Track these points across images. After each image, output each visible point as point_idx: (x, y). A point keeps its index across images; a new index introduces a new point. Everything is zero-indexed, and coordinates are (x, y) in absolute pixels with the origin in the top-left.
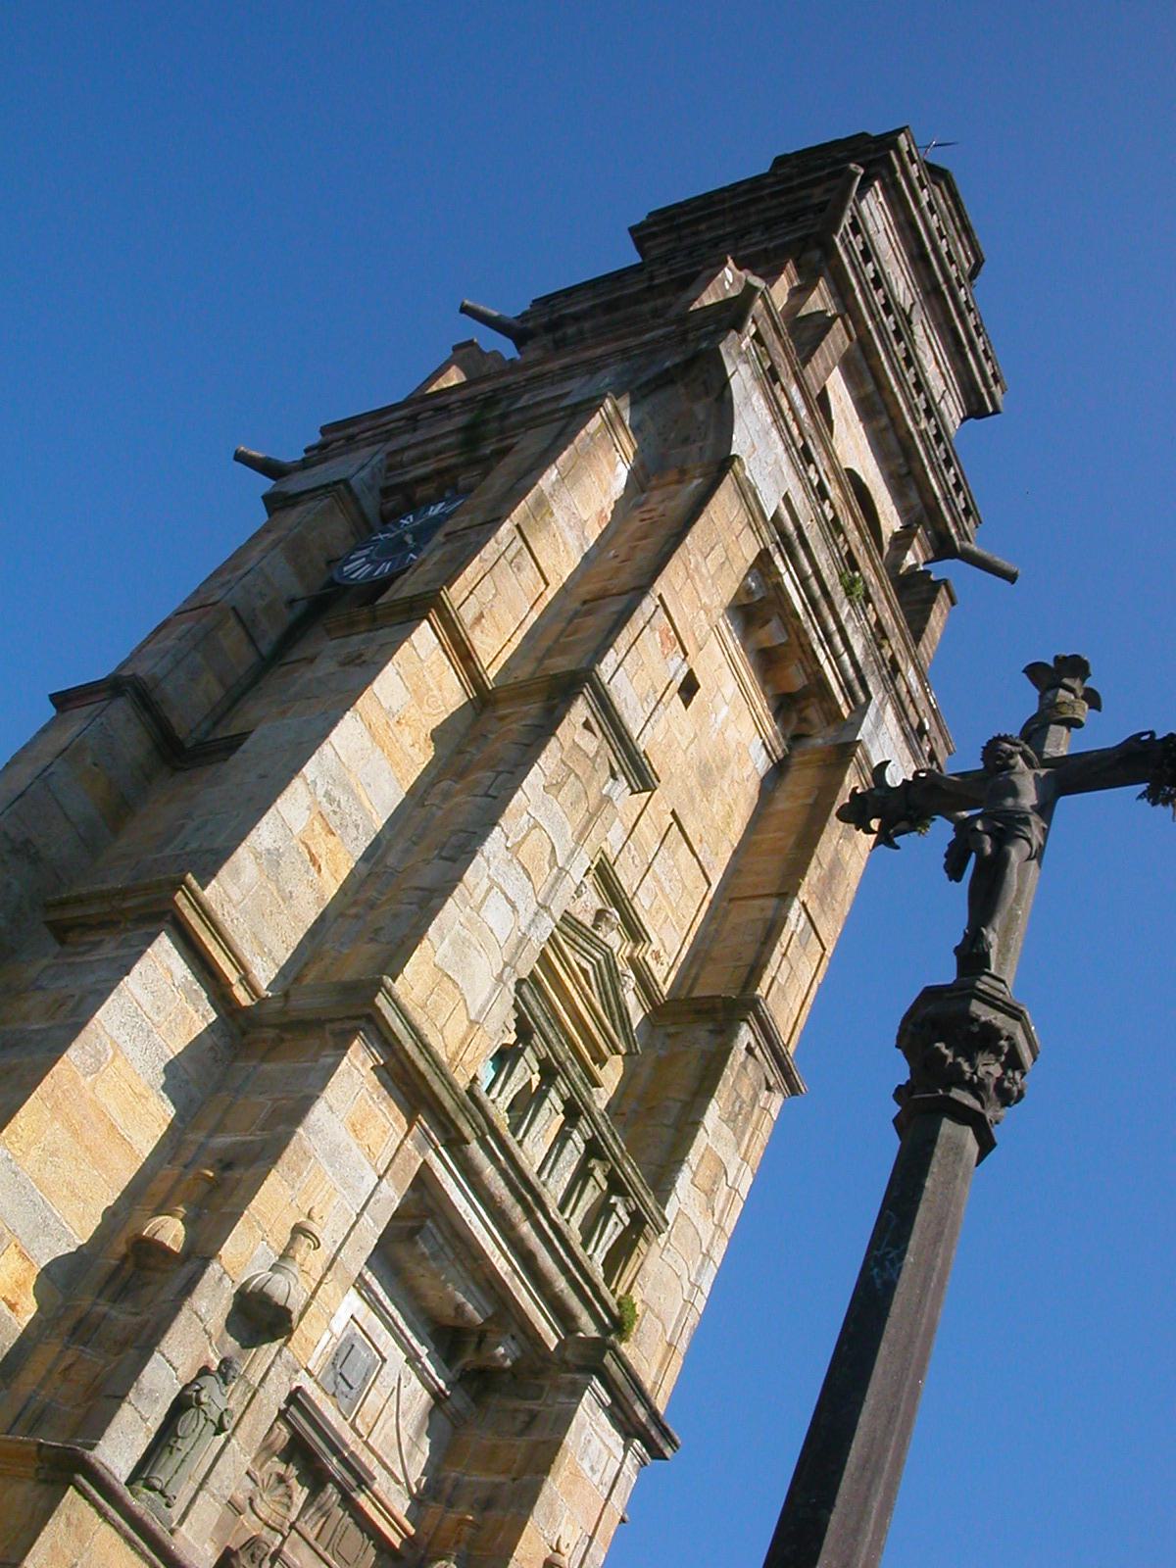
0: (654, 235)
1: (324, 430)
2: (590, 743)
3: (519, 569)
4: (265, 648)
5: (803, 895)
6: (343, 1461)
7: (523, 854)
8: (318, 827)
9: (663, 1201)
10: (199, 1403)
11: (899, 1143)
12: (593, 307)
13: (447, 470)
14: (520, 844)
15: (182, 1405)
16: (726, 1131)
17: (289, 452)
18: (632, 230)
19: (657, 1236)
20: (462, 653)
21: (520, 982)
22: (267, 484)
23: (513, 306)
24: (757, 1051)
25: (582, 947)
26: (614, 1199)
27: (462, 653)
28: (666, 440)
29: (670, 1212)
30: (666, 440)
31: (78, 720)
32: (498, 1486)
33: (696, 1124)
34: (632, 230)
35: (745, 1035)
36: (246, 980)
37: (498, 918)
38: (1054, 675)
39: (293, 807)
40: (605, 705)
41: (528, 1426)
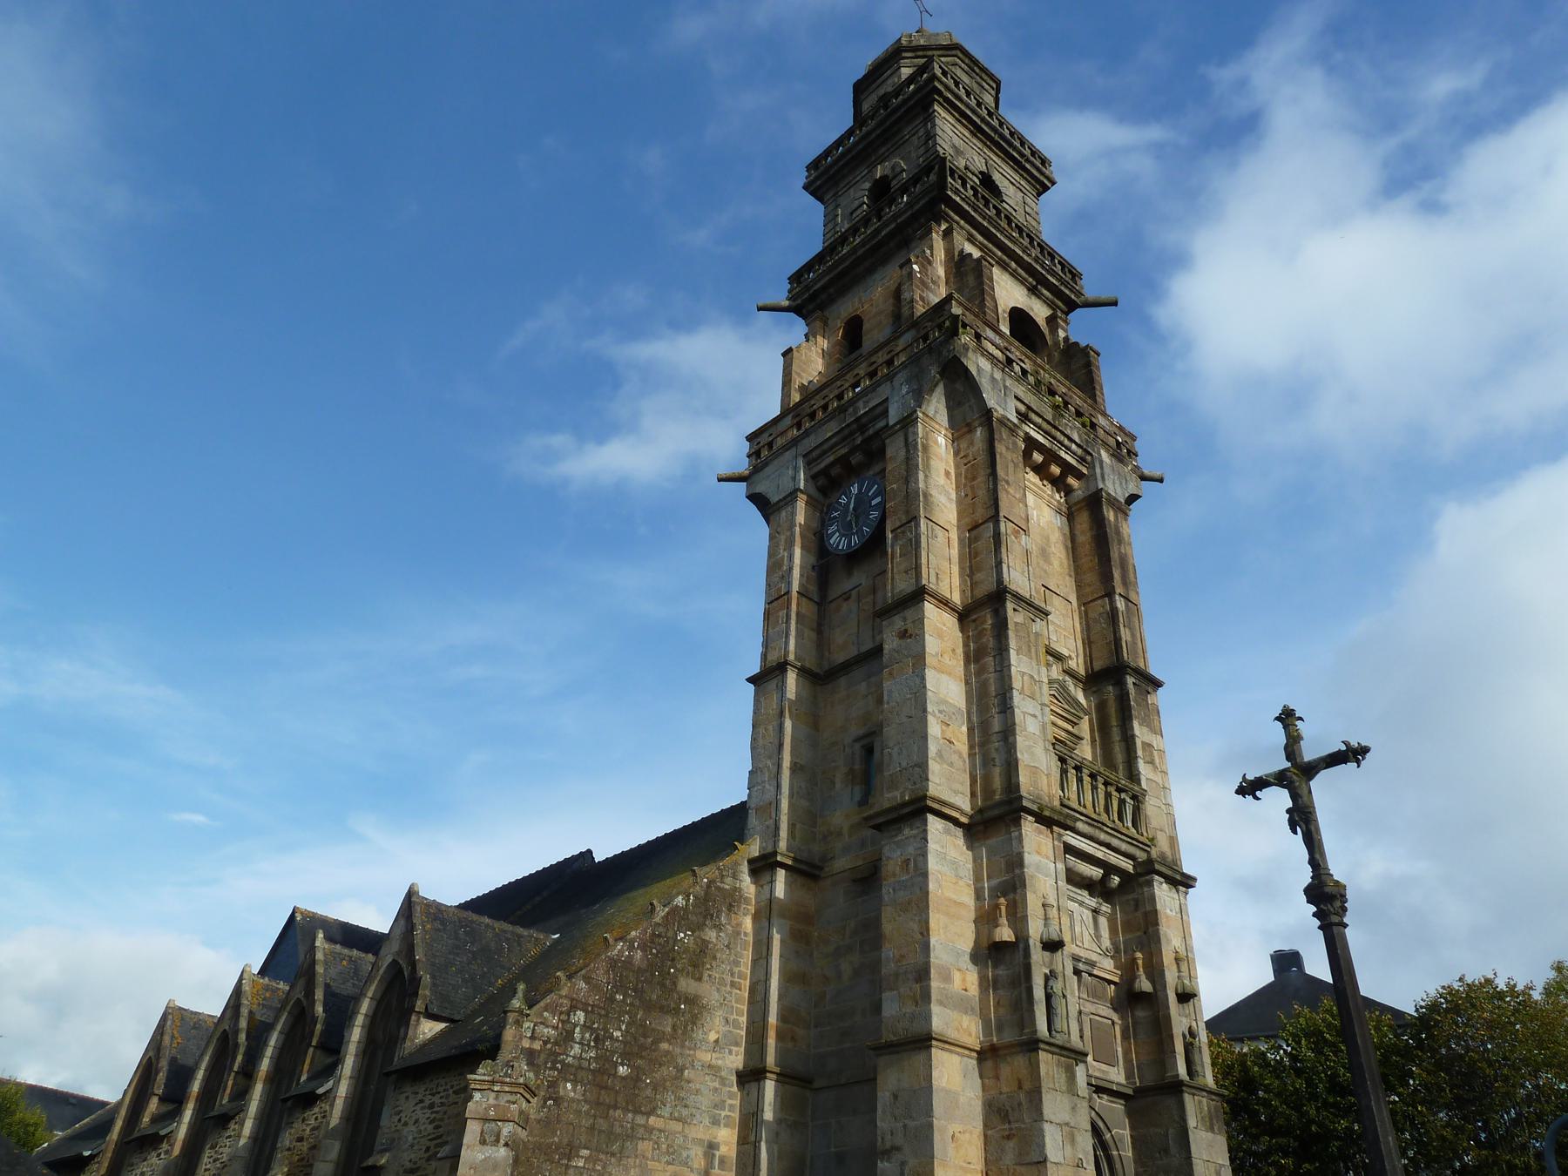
0: (819, 187)
5: (1118, 590)
11: (1363, 992)
18: (806, 188)
20: (944, 603)
25: (825, 452)
27: (944, 603)
29: (1144, 786)
33: (1133, 736)
34: (806, 188)
35: (1130, 680)
36: (962, 812)
38: (1287, 717)
39: (934, 728)
40: (1018, 598)
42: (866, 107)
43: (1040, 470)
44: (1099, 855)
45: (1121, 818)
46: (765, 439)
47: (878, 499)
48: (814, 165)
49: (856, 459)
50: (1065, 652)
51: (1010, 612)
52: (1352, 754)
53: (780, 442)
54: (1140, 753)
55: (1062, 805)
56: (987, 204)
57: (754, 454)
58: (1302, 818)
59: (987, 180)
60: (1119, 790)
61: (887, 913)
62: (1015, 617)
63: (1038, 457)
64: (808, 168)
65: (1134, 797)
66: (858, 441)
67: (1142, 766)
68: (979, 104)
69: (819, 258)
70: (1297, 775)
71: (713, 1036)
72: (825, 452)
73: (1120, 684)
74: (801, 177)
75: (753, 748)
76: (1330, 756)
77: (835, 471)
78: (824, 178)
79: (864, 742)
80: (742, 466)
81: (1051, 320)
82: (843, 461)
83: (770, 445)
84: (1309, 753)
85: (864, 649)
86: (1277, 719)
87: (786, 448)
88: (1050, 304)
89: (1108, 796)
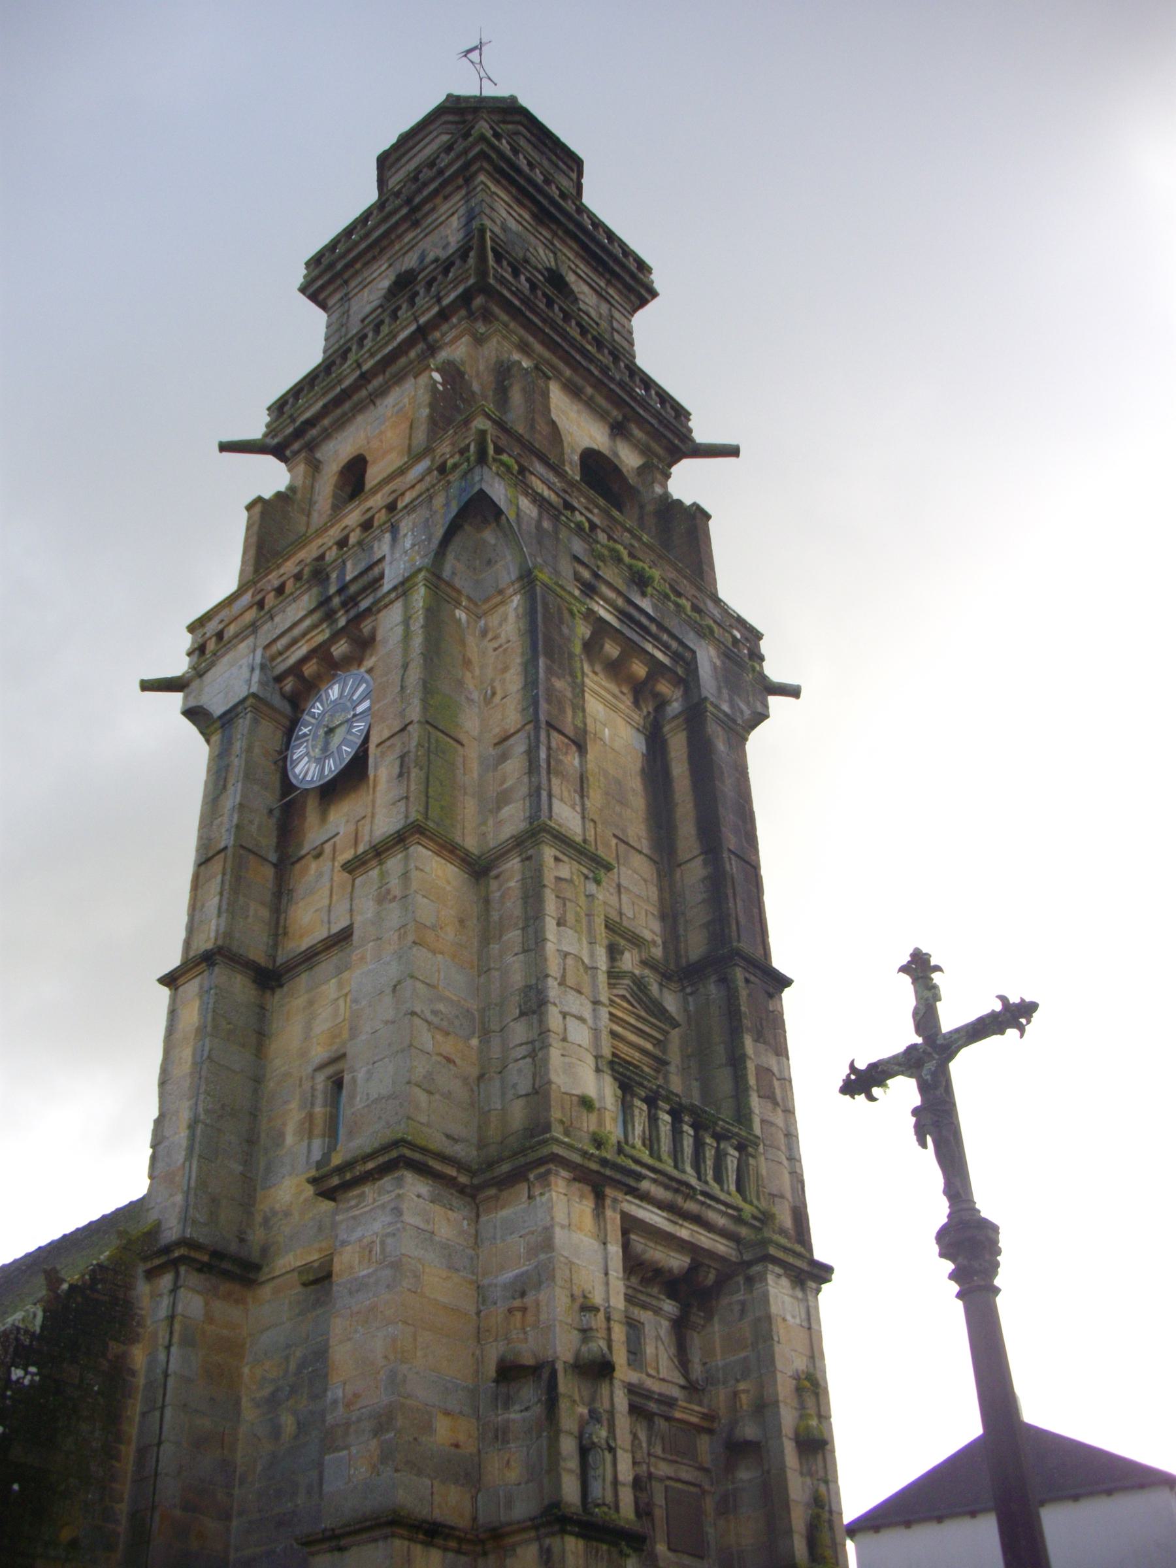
0: (322, 288)
1: (192, 628)
2: (565, 871)
3: (444, 753)
4: (273, 857)
6: (658, 1401)
7: (571, 981)
8: (439, 1037)
9: (750, 1128)
10: (593, 1443)
11: (945, 1220)
12: (325, 406)
13: (320, 646)
14: (564, 976)
15: (585, 1450)
16: (761, 1047)
17: (178, 665)
18: (303, 290)
19: (756, 1150)
21: (611, 1063)
22: (176, 699)
23: (255, 427)
24: (752, 978)
25: (294, 642)
26: (722, 1146)
28: (475, 569)
29: (757, 1130)
30: (475, 569)
31: (191, 988)
32: (745, 1359)
33: (743, 1057)
34: (303, 290)
35: (739, 974)
37: (580, 1034)
38: (920, 968)
41: (743, 1312)
42: (393, 182)
43: (615, 669)
44: (684, 1234)
45: (719, 1178)
46: (213, 627)
47: (366, 704)
48: (315, 262)
49: (340, 649)
50: (647, 935)
51: (549, 861)
52: (1013, 1016)
53: (231, 630)
54: (752, 1081)
55: (620, 1151)
56: (550, 303)
57: (198, 650)
58: (937, 1122)
59: (556, 280)
60: (718, 1137)
61: (338, 1326)
62: (556, 867)
63: (612, 650)
64: (308, 264)
65: (741, 1148)
66: (342, 622)
67: (755, 1101)
68: (547, 181)
69: (311, 380)
70: (929, 1059)
71: (66, 1535)
72: (294, 642)
73: (725, 981)
74: (299, 274)
75: (162, 1083)
76: (981, 1020)
77: (309, 669)
78: (327, 277)
79: (330, 1070)
80: (178, 665)
81: (642, 470)
82: (321, 652)
83: (220, 635)
84: (952, 1016)
85: (335, 929)
86: (903, 969)
87: (240, 636)
88: (645, 451)
89: (699, 1145)
